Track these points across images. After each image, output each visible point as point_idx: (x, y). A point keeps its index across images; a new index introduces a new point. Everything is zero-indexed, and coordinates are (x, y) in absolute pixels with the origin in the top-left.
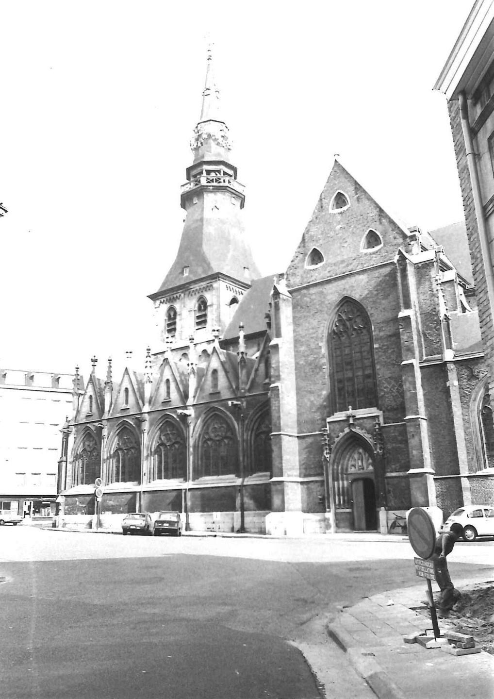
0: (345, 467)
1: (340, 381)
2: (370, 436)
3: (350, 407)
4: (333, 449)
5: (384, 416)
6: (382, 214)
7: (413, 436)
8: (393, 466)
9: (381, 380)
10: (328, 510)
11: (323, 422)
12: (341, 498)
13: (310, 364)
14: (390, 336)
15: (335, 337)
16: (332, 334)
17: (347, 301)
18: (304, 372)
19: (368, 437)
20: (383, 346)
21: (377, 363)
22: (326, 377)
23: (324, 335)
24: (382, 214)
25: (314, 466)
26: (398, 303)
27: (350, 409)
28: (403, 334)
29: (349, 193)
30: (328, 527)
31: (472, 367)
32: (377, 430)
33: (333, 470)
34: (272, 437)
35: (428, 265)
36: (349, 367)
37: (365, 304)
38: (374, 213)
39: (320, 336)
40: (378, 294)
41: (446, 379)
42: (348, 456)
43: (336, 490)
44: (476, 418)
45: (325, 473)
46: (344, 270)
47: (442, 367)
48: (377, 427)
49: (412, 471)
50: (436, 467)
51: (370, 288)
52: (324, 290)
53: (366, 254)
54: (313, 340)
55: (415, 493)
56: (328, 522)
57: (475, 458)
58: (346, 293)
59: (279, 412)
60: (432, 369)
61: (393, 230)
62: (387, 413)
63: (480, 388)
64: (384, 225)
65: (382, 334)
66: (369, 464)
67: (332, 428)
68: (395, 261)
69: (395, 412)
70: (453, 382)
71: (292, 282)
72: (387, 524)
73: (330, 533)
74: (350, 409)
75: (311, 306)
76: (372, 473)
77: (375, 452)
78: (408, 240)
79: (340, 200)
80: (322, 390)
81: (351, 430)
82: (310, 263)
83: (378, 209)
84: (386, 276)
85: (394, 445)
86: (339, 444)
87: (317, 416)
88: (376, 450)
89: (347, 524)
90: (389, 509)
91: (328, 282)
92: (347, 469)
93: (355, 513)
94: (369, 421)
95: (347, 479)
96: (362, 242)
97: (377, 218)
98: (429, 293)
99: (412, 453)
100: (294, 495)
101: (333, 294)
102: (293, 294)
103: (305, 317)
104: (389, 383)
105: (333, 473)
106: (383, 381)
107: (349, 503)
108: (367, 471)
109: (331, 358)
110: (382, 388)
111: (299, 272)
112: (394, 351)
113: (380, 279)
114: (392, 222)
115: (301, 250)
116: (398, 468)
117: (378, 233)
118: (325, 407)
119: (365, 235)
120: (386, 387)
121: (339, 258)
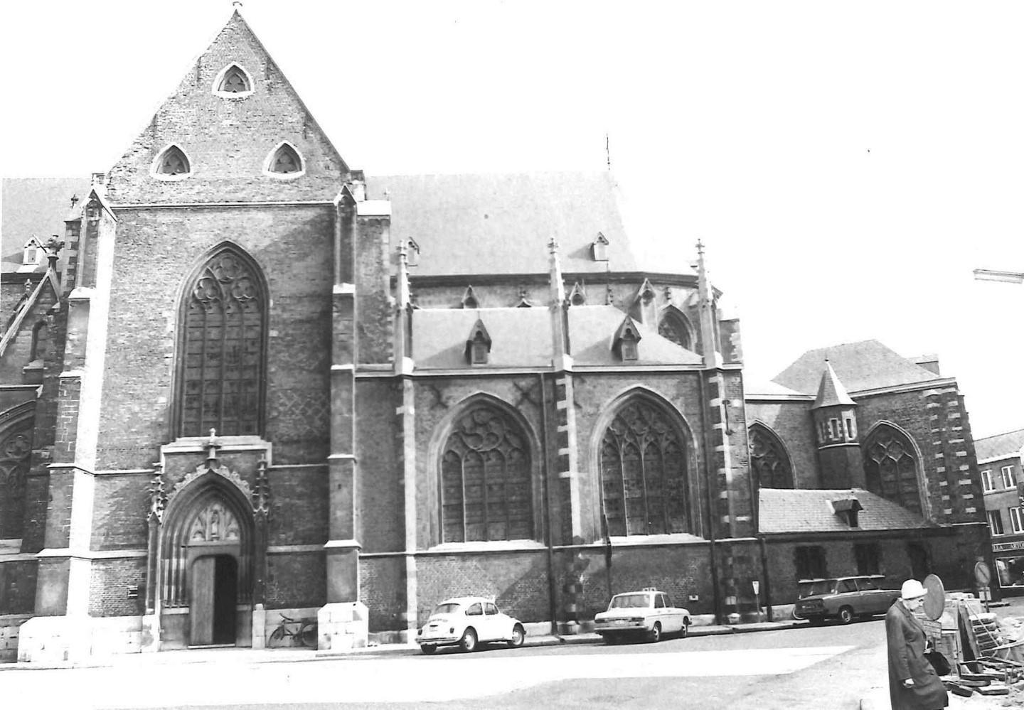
0: (184, 533)
1: (193, 384)
2: (245, 483)
3: (213, 430)
4: (170, 501)
5: (273, 450)
6: (310, 124)
7: (340, 486)
8: (283, 536)
9: (275, 392)
10: (149, 610)
11: (154, 453)
12: (173, 588)
13: (139, 347)
14: (301, 321)
15: (195, 306)
16: (190, 301)
17: (229, 251)
18: (130, 357)
19: (244, 486)
20: (287, 335)
21: (272, 362)
22: (170, 374)
23: (175, 299)
24: (310, 124)
25: (134, 529)
26: (332, 270)
27: (213, 434)
28: (338, 322)
29: (255, 73)
30: (146, 641)
31: (440, 389)
32: (262, 474)
33: (164, 537)
34: (52, 472)
35: (379, 222)
36: (214, 362)
37: (263, 261)
38: (297, 117)
39: (168, 299)
40: (287, 250)
41: (400, 402)
42: (191, 516)
43: (166, 574)
44: (433, 466)
45: (149, 542)
46: (228, 197)
47: (392, 386)
48: (262, 468)
49: (331, 544)
50: (365, 541)
51: (276, 237)
52: (186, 222)
53: (272, 181)
54: (153, 305)
55: (334, 580)
56: (148, 633)
57: (428, 528)
58: (232, 237)
59: (74, 424)
60: (374, 384)
61: (324, 154)
62: (280, 448)
63: (446, 424)
64: (311, 142)
65: (285, 316)
66: (232, 531)
67: (172, 464)
68: (336, 203)
69: (294, 446)
70: (408, 409)
71: (118, 193)
72: (265, 631)
73: (152, 652)
74: (213, 434)
75: (155, 244)
76: (235, 546)
77: (256, 511)
78: (349, 176)
79: (236, 78)
80: (160, 394)
81: (211, 471)
82: (161, 170)
83: (303, 114)
84: (305, 223)
85: (287, 500)
86: (183, 493)
87: (144, 441)
88: (256, 506)
89: (180, 634)
90: (270, 606)
91: (197, 209)
92: (187, 538)
93: (194, 616)
94: (248, 457)
95: (185, 557)
96: (267, 158)
97: (300, 127)
98: (377, 265)
99: (334, 514)
100: (85, 582)
101: (205, 233)
102: (121, 215)
103: (139, 260)
104: (290, 399)
105: (164, 543)
106: (280, 394)
107: (184, 597)
108: (225, 543)
109: (181, 340)
110: (276, 405)
111: (137, 179)
112: (305, 347)
113: (295, 226)
114: (325, 141)
115: (148, 141)
116: (290, 539)
117: (299, 153)
118: (160, 425)
119: (275, 150)
120: (282, 405)
121: (222, 175)
